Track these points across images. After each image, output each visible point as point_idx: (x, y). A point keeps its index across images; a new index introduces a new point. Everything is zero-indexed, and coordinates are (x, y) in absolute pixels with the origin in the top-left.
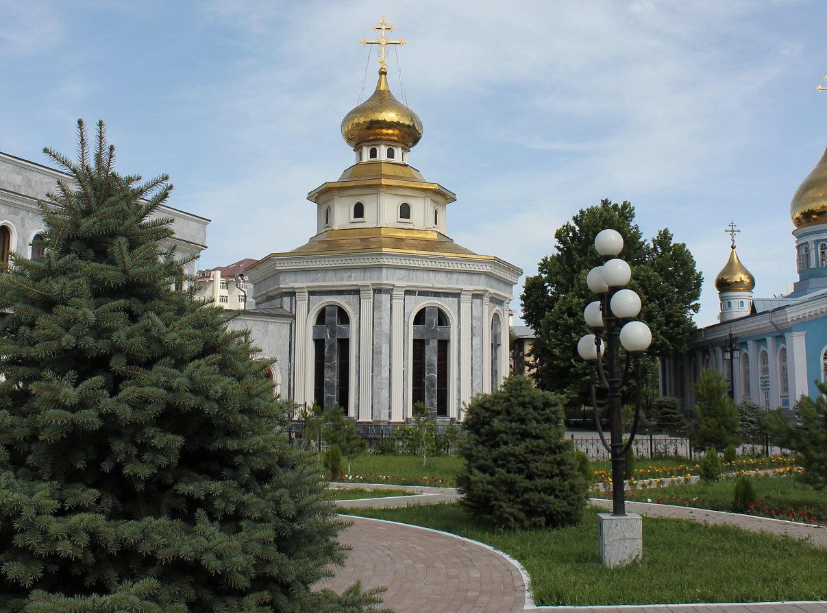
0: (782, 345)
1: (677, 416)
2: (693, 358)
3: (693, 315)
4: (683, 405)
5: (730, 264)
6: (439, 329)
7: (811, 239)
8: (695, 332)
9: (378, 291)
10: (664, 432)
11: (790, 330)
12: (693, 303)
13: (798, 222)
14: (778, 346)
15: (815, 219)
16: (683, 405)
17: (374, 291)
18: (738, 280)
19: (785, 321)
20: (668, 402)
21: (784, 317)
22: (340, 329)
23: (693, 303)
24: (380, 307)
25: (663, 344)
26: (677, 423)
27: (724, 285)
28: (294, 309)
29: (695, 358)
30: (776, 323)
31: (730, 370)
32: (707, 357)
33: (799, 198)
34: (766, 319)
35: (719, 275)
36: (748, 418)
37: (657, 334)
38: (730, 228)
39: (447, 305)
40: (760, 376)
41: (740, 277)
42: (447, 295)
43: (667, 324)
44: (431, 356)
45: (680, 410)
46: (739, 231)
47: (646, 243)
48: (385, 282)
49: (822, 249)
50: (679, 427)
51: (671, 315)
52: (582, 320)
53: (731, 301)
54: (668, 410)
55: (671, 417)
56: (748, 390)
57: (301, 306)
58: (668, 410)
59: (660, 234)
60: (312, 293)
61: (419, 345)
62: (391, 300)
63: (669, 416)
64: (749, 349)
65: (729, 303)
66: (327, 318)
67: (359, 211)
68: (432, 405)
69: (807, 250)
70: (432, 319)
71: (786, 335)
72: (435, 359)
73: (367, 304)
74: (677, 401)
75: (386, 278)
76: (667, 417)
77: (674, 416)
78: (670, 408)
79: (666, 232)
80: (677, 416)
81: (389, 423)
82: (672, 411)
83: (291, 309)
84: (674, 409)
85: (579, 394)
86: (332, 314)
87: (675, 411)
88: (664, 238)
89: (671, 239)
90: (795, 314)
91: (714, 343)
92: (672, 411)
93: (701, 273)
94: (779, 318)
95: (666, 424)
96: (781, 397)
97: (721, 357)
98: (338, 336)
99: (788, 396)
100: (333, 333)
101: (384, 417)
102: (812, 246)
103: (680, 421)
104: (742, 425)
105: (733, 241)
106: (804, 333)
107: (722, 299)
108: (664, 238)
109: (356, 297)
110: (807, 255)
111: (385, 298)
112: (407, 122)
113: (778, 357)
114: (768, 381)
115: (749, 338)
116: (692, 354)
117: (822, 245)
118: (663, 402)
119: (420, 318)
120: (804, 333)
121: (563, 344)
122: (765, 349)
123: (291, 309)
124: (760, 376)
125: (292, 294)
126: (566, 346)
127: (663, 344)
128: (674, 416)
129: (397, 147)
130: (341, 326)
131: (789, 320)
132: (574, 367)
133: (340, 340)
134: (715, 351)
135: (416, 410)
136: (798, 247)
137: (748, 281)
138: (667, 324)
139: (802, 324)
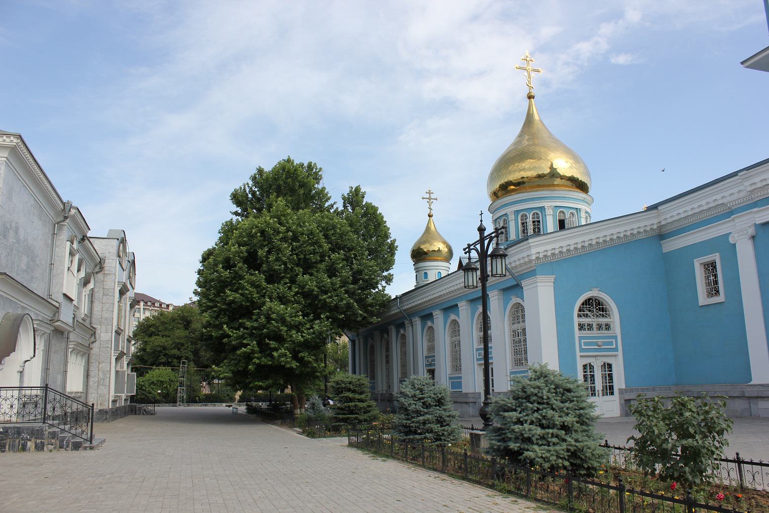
0: (515, 300)
1: (365, 404)
2: (385, 335)
3: (385, 287)
4: (373, 388)
7: (509, 210)
8: (387, 303)
10: (343, 432)
11: (532, 273)
12: (385, 274)
15: (513, 190)
16: (373, 388)
18: (436, 249)
19: (526, 260)
20: (350, 383)
21: (525, 254)
23: (385, 274)
25: (349, 306)
26: (365, 416)
27: (419, 255)
29: (388, 335)
32: (402, 331)
33: (493, 176)
35: (413, 247)
36: (558, 421)
37: (341, 292)
38: (427, 196)
40: (475, 347)
41: (438, 246)
43: (355, 282)
45: (369, 394)
47: (335, 207)
50: (369, 421)
51: (360, 272)
53: (428, 272)
54: (351, 395)
55: (356, 406)
56: (457, 366)
58: (351, 395)
59: (351, 192)
63: (353, 404)
65: (426, 273)
71: (524, 283)
74: (366, 381)
76: (349, 407)
77: (361, 405)
78: (354, 391)
79: (357, 190)
80: (365, 404)
82: (357, 396)
84: (361, 393)
85: (233, 372)
87: (363, 396)
88: (354, 198)
89: (363, 197)
90: (541, 249)
91: (411, 314)
92: (357, 396)
93: (395, 240)
94: (515, 258)
95: (348, 418)
96: (450, 378)
97: (416, 330)
99: (460, 378)
103: (369, 412)
104: (542, 438)
106: (552, 278)
107: (417, 270)
108: (354, 198)
113: (506, 318)
114: (434, 360)
115: (435, 307)
116: (383, 329)
117: (522, 216)
118: (343, 382)
120: (552, 278)
121: (216, 306)
126: (221, 310)
127: (349, 306)
128: (361, 405)
131: (534, 257)
132: (228, 336)
134: (412, 324)
137: (446, 250)
138: (355, 282)
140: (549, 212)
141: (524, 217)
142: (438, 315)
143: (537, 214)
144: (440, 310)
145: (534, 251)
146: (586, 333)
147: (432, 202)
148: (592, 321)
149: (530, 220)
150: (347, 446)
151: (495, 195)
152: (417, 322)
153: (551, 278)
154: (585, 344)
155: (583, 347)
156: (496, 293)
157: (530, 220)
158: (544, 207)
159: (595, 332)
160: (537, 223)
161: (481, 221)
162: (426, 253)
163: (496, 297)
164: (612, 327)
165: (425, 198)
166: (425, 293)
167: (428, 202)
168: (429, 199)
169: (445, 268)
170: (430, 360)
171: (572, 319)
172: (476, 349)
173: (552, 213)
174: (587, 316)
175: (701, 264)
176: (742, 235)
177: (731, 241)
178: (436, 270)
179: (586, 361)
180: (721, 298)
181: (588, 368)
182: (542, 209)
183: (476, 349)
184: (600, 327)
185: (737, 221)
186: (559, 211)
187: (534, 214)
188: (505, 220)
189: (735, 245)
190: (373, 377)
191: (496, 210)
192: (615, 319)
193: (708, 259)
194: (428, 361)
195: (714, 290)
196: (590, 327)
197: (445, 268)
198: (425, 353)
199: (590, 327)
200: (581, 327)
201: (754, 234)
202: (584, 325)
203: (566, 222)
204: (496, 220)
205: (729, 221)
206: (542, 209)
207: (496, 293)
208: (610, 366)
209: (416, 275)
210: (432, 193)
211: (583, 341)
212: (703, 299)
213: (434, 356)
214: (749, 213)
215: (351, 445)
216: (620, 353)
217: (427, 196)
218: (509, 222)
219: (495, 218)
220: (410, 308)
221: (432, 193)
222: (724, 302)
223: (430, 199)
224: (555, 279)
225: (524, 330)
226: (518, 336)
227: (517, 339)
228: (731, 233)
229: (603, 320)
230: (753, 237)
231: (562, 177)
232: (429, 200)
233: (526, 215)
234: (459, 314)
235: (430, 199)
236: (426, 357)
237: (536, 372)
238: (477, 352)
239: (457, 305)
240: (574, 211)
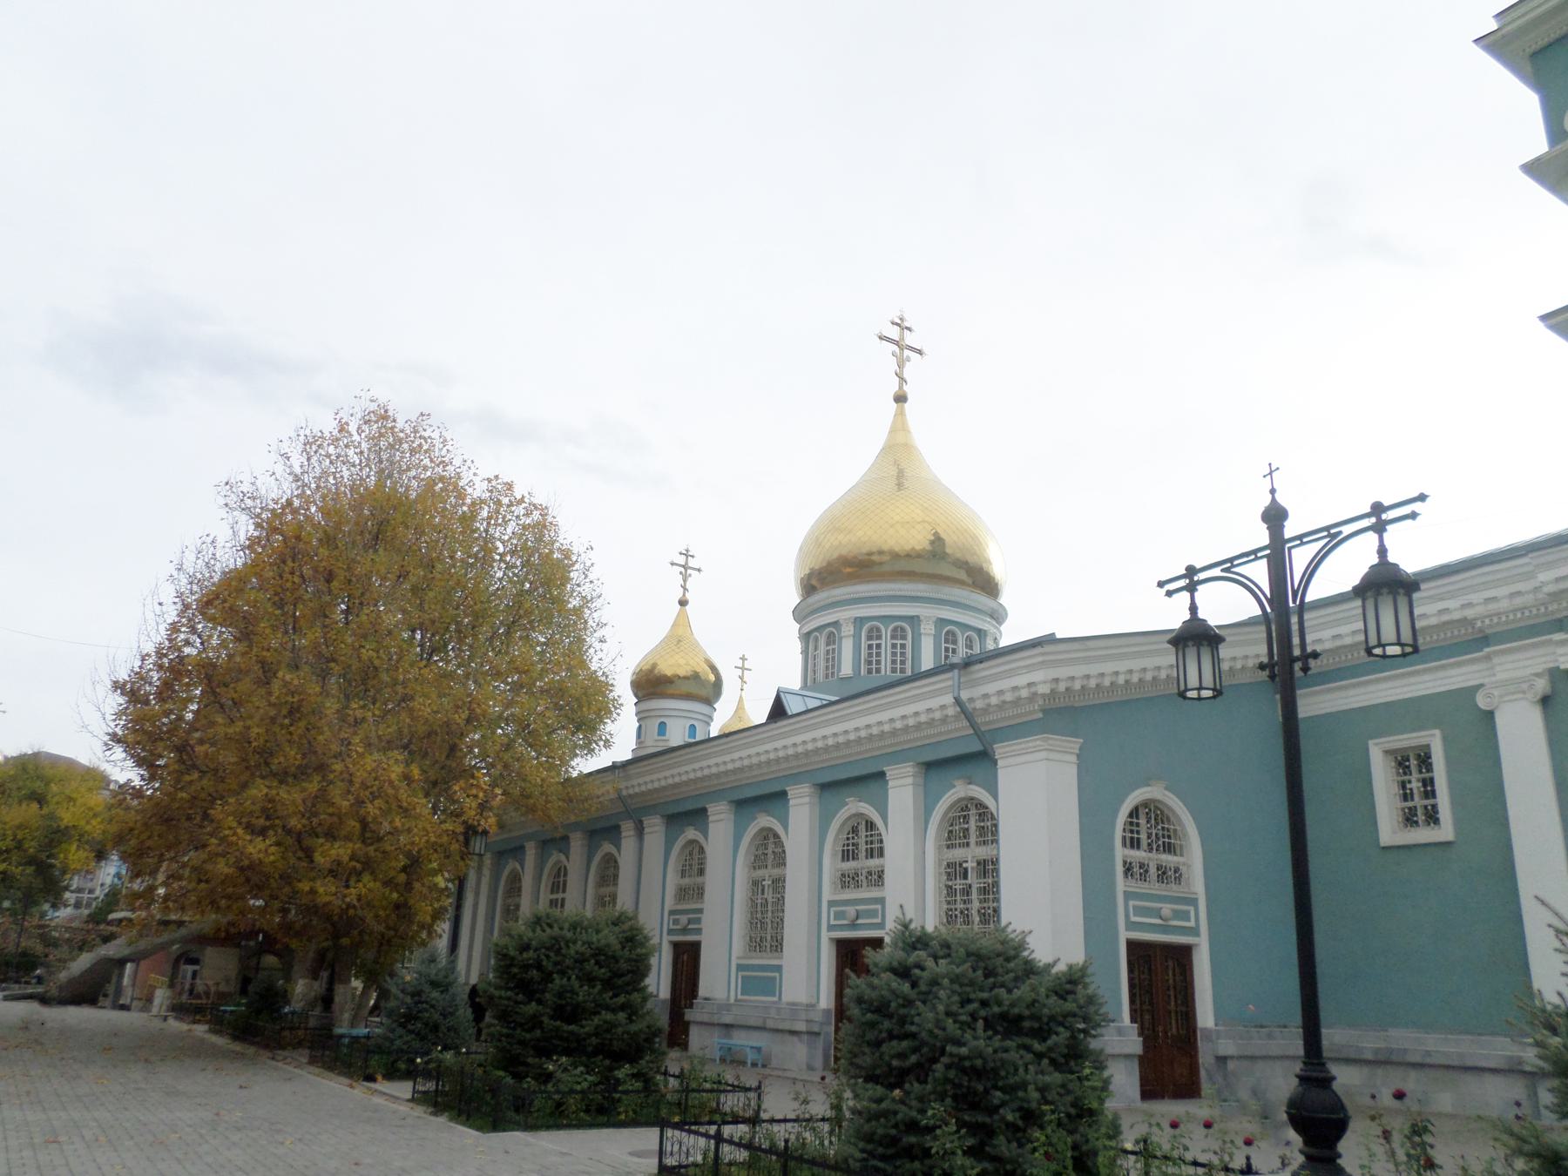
7: (845, 614)
30: (970, 706)
31: (1369, 1056)
34: (940, 692)
38: (681, 560)
46: (699, 570)
49: (869, 638)
52: (1029, 967)
64: (572, 850)
71: (1000, 750)
96: (740, 968)
102: (848, 630)
105: (685, 589)
106: (1075, 744)
114: (698, 921)
115: (716, 795)
117: (871, 630)
120: (1075, 744)
122: (613, 850)
134: (640, 831)
136: (806, 637)
142: (721, 821)
143: (903, 630)
144: (662, 816)
147: (908, 359)
148: (1149, 859)
150: (408, 1101)
151: (810, 585)
152: (655, 828)
153: (1072, 745)
154: (1140, 911)
155: (1134, 919)
156: (807, 790)
158: (918, 617)
161: (1273, 491)
163: (807, 799)
164: (1185, 876)
165: (677, 564)
166: (697, 760)
167: (681, 573)
168: (683, 566)
169: (701, 717)
170: (684, 919)
171: (1112, 849)
172: (829, 902)
173: (933, 632)
175: (1387, 752)
176: (1513, 693)
177: (1482, 702)
178: (685, 721)
180: (1446, 831)
182: (914, 621)
183: (829, 902)
185: (1496, 660)
186: (946, 630)
187: (895, 630)
188: (831, 635)
189: (1490, 715)
190: (121, 963)
191: (805, 618)
192: (1194, 858)
193: (1407, 740)
194: (676, 922)
195: (1420, 812)
197: (701, 717)
198: (670, 903)
200: (1128, 870)
201: (1548, 690)
202: (870, 884)
204: (809, 634)
205: (1472, 661)
207: (908, 769)
209: (640, 727)
210: (692, 556)
211: (1131, 903)
212: (1389, 830)
213: (700, 911)
214: (1543, 644)
215: (419, 1099)
217: (681, 560)
218: (841, 638)
219: (806, 630)
220: (650, 790)
221: (692, 556)
222: (1448, 844)
223: (685, 567)
224: (1080, 749)
225: (563, 900)
226: (763, 894)
227: (959, 884)
228: (1482, 685)
229: (1168, 859)
230: (1545, 701)
232: (683, 570)
233: (878, 630)
234: (569, 849)
235: (685, 567)
236: (672, 913)
238: (672, 917)
239: (703, 811)
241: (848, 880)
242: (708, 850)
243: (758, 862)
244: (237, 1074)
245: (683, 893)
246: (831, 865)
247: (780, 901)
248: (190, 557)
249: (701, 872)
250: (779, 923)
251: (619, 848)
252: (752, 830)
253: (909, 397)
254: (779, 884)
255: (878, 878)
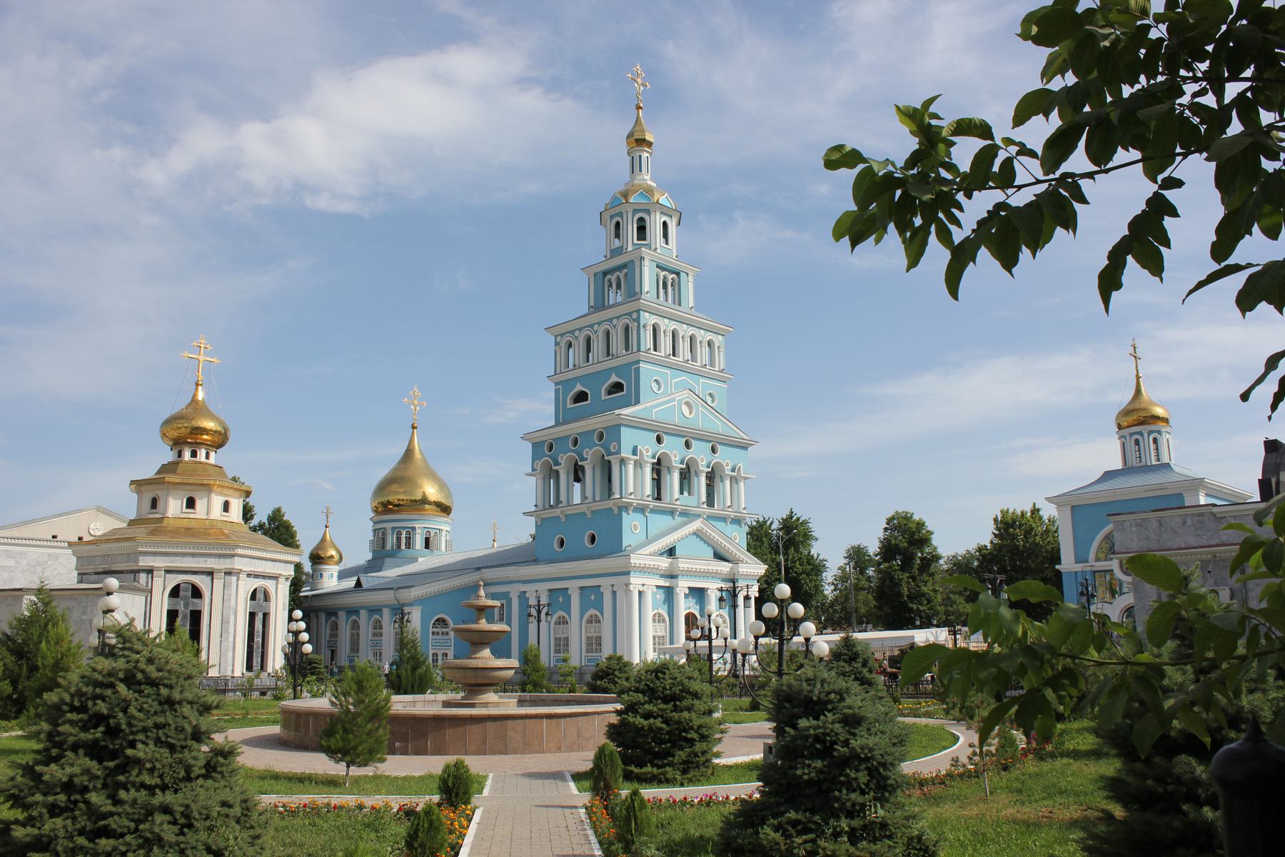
5: (323, 540)
6: (264, 604)
9: (228, 573)
13: (376, 511)
14: (370, 618)
15: (390, 509)
17: (225, 573)
22: (193, 603)
24: (230, 586)
28: (150, 584)
39: (270, 585)
40: (370, 638)
42: (270, 577)
44: (258, 625)
48: (236, 567)
57: (158, 582)
60: (168, 572)
61: (252, 616)
62: (238, 581)
65: (321, 574)
66: (182, 593)
67: (191, 503)
68: (257, 663)
69: (384, 534)
70: (260, 596)
72: (261, 627)
73: (218, 584)
75: (238, 564)
81: (233, 677)
83: (147, 583)
86: (186, 590)
90: (416, 593)
98: (191, 608)
100: (186, 605)
101: (229, 674)
109: (209, 578)
110: (383, 538)
111: (234, 578)
112: (219, 429)
115: (341, 609)
119: (175, 592)
123: (147, 583)
124: (370, 638)
125: (150, 571)
129: (212, 451)
130: (194, 600)
133: (192, 612)
134: (317, 616)
135: (249, 667)
136: (375, 531)
139: (418, 601)
140: (418, 531)
141: (399, 534)
145: (413, 594)
146: (435, 637)
149: (404, 536)
152: (323, 616)
157: (404, 536)
159: (440, 637)
160: (408, 539)
162: (322, 558)
174: (437, 627)
179: (434, 652)
181: (435, 655)
184: (443, 634)
196: (438, 633)
198: (328, 638)
199: (438, 633)
200: (433, 633)
203: (431, 539)
206: (414, 529)
208: (446, 654)
216: (452, 648)
229: (445, 630)
231: (430, 503)
237: (934, 846)
240: (438, 531)
241: (375, 635)
242: (339, 624)
243: (353, 628)
244: (655, 663)
245: (331, 636)
246: (371, 630)
247: (358, 639)
248: (995, 531)
249: (337, 630)
250: (358, 644)
251: (359, 618)
252: (329, 621)
253: (856, 543)
254: (358, 635)
255: (381, 635)
